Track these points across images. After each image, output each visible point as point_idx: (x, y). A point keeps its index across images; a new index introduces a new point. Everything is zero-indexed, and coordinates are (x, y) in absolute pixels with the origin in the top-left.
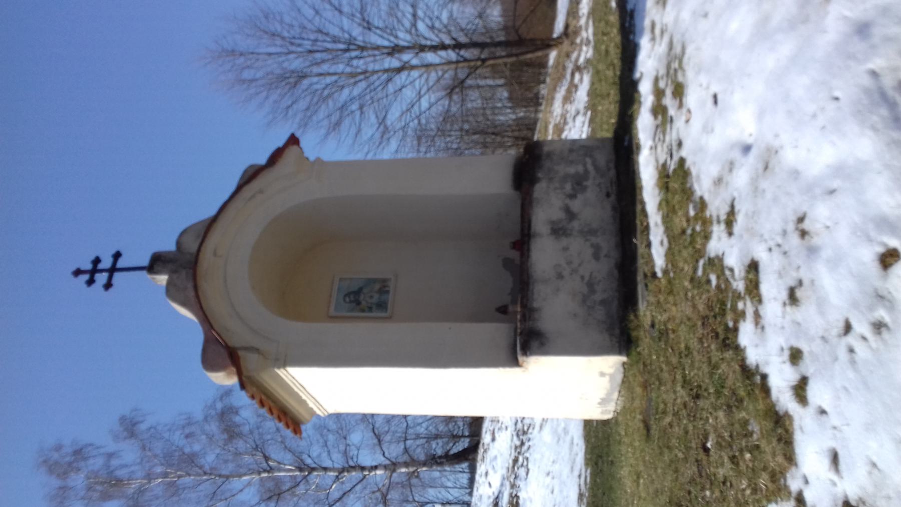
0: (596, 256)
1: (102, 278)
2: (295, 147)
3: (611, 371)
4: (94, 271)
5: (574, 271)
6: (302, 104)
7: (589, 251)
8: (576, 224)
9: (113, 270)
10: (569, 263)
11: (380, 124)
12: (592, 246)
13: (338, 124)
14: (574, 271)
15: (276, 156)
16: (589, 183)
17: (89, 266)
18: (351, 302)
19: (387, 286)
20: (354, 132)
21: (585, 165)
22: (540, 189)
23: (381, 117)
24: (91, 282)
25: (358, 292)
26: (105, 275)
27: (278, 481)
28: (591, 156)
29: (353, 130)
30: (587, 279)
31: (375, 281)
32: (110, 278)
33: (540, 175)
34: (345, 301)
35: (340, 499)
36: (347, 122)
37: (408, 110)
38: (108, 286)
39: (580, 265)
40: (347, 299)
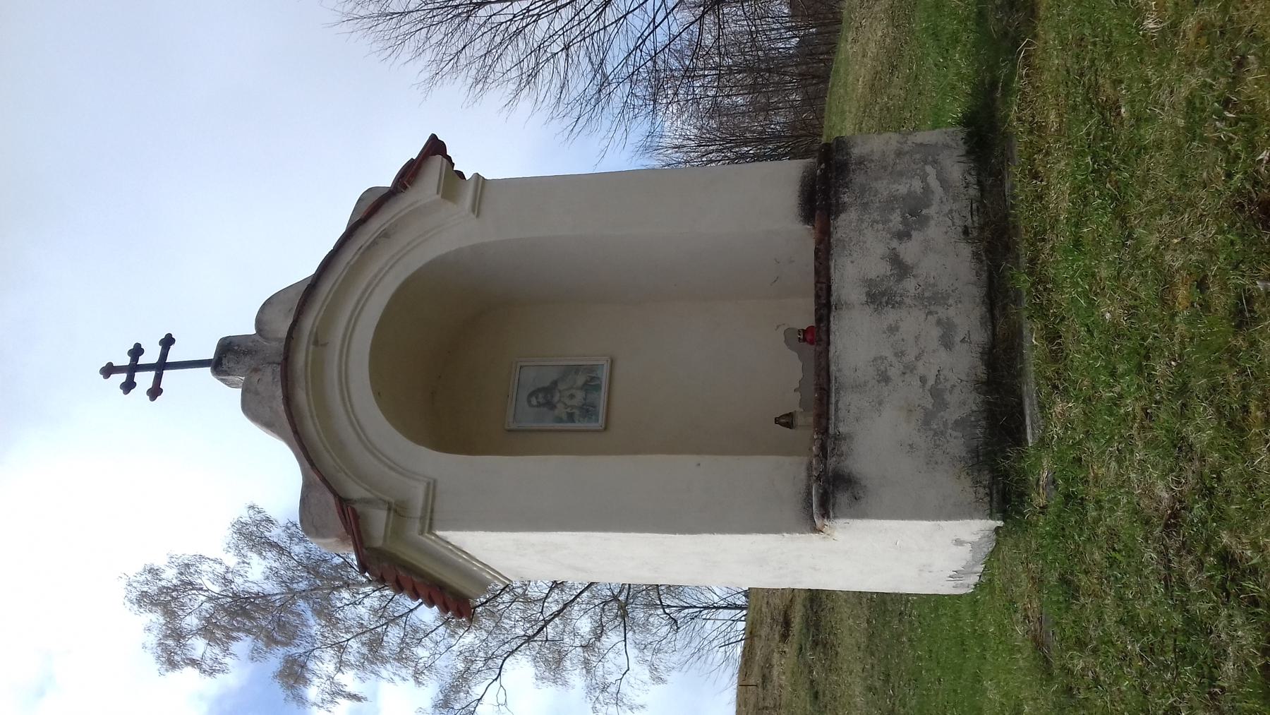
0: (947, 342)
1: (144, 380)
2: (439, 158)
3: (976, 538)
5: (909, 369)
6: (479, 47)
7: (936, 332)
8: (910, 285)
9: (161, 366)
10: (900, 354)
11: (596, 72)
13: (534, 74)
14: (909, 369)
15: (410, 174)
17: (126, 361)
18: (539, 405)
20: (558, 86)
21: (924, 179)
22: (845, 224)
23: (596, 61)
24: (128, 386)
25: (549, 390)
26: (151, 375)
28: (935, 162)
29: (557, 82)
30: (931, 382)
31: (577, 369)
32: (158, 379)
33: (846, 198)
34: (529, 401)
35: (560, 611)
36: (546, 72)
37: (636, 48)
38: (155, 392)
40: (534, 401)
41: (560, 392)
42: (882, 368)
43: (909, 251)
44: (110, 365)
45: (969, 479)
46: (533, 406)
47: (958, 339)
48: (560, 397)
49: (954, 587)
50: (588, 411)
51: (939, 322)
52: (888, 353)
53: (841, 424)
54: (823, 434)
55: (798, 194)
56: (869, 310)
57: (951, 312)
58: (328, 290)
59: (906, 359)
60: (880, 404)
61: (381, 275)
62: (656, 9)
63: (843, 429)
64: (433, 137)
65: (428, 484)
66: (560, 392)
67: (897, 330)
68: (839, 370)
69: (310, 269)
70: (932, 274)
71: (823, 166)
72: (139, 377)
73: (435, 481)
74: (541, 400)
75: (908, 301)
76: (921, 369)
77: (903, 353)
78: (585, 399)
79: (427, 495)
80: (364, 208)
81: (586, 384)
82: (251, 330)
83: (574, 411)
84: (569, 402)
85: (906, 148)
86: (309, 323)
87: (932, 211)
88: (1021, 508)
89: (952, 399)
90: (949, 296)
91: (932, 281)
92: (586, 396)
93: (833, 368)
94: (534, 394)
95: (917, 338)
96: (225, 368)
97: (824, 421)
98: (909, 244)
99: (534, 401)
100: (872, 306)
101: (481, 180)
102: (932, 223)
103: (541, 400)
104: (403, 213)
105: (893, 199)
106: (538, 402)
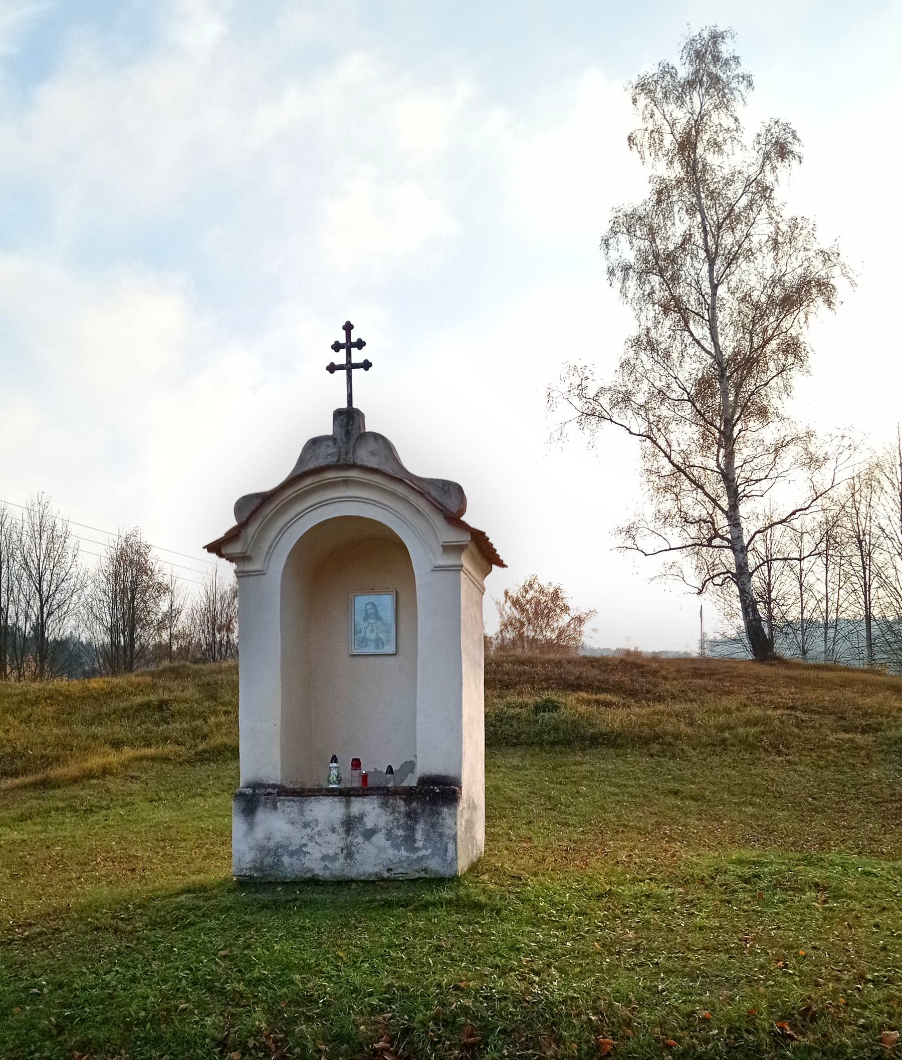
1: (340, 358)
5: (311, 838)
7: (331, 852)
8: (360, 839)
10: (319, 834)
12: (337, 854)
16: (403, 853)
18: (366, 610)
19: (23, 776)
24: (337, 347)
39: (316, 842)
40: (369, 607)
42: (312, 824)
44: (360, 348)
47: (326, 863)
55: (428, 773)
57: (342, 860)
59: (316, 837)
68: (311, 802)
74: (370, 611)
76: (310, 844)
79: (255, 571)
84: (369, 629)
85: (444, 839)
89: (294, 860)
90: (352, 859)
94: (374, 606)
95: (328, 843)
96: (338, 418)
97: (283, 794)
98: (384, 840)
99: (369, 607)
103: (370, 611)
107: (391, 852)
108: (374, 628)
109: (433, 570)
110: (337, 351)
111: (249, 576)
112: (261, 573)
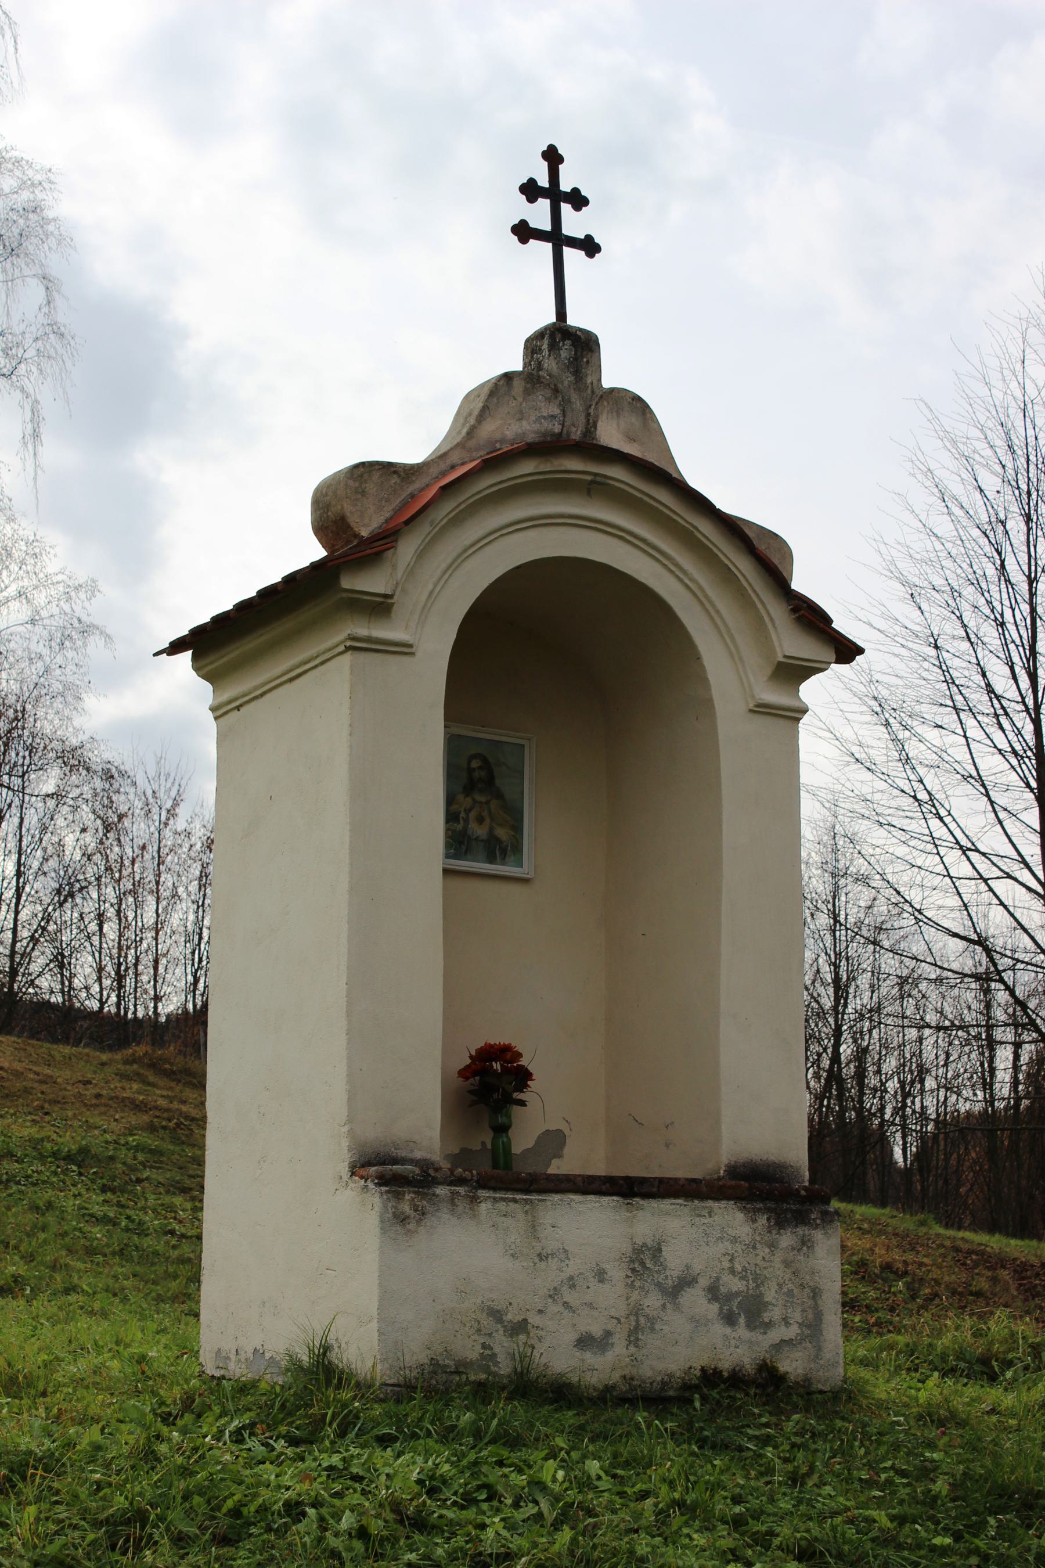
0: (584, 1342)
1: (539, 215)
4: (555, 195)
7: (597, 1331)
8: (653, 1301)
9: (557, 238)
10: (572, 1283)
18: (470, 771)
24: (530, 190)
27: (729, 1268)
39: (566, 1304)
40: (475, 764)
41: (487, 803)
43: (695, 1300)
45: (426, 1361)
46: (469, 762)
48: (480, 802)
49: (219, 1350)
50: (461, 843)
51: (608, 1334)
52: (572, 1268)
53: (490, 1205)
54: (477, 1182)
56: (628, 1249)
58: (661, 498)
59: (565, 1290)
60: (513, 1255)
61: (678, 573)
62: (995, 859)
63: (484, 1207)
64: (860, 651)
65: (411, 646)
66: (487, 803)
67: (600, 1281)
69: (695, 481)
70: (666, 1328)
71: (803, 1193)
72: (544, 205)
73: (413, 654)
74: (476, 775)
75: (635, 1295)
77: (573, 1286)
78: (477, 839)
80: (761, 547)
81: (498, 840)
82: (607, 382)
83: (461, 821)
84: (472, 815)
86: (616, 473)
87: (742, 1331)
88: (495, 1393)
91: (657, 1327)
92: (482, 841)
93: (556, 1197)
99: (475, 764)
100: (630, 1249)
101: (797, 715)
102: (728, 1330)
104: (759, 606)
105: (759, 1280)
106: (474, 769)
107: (719, 1329)
108: (485, 813)
109: (751, 711)
110: (531, 200)
111: (732, 657)
112: (404, 649)
